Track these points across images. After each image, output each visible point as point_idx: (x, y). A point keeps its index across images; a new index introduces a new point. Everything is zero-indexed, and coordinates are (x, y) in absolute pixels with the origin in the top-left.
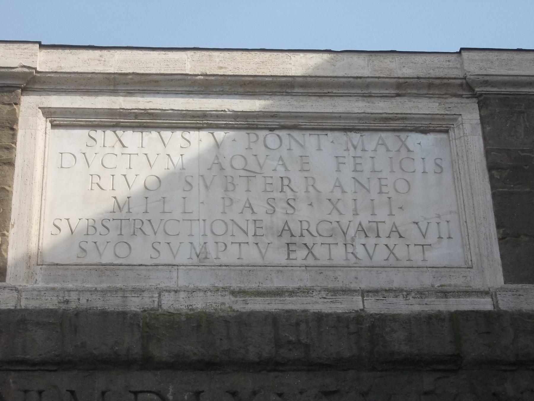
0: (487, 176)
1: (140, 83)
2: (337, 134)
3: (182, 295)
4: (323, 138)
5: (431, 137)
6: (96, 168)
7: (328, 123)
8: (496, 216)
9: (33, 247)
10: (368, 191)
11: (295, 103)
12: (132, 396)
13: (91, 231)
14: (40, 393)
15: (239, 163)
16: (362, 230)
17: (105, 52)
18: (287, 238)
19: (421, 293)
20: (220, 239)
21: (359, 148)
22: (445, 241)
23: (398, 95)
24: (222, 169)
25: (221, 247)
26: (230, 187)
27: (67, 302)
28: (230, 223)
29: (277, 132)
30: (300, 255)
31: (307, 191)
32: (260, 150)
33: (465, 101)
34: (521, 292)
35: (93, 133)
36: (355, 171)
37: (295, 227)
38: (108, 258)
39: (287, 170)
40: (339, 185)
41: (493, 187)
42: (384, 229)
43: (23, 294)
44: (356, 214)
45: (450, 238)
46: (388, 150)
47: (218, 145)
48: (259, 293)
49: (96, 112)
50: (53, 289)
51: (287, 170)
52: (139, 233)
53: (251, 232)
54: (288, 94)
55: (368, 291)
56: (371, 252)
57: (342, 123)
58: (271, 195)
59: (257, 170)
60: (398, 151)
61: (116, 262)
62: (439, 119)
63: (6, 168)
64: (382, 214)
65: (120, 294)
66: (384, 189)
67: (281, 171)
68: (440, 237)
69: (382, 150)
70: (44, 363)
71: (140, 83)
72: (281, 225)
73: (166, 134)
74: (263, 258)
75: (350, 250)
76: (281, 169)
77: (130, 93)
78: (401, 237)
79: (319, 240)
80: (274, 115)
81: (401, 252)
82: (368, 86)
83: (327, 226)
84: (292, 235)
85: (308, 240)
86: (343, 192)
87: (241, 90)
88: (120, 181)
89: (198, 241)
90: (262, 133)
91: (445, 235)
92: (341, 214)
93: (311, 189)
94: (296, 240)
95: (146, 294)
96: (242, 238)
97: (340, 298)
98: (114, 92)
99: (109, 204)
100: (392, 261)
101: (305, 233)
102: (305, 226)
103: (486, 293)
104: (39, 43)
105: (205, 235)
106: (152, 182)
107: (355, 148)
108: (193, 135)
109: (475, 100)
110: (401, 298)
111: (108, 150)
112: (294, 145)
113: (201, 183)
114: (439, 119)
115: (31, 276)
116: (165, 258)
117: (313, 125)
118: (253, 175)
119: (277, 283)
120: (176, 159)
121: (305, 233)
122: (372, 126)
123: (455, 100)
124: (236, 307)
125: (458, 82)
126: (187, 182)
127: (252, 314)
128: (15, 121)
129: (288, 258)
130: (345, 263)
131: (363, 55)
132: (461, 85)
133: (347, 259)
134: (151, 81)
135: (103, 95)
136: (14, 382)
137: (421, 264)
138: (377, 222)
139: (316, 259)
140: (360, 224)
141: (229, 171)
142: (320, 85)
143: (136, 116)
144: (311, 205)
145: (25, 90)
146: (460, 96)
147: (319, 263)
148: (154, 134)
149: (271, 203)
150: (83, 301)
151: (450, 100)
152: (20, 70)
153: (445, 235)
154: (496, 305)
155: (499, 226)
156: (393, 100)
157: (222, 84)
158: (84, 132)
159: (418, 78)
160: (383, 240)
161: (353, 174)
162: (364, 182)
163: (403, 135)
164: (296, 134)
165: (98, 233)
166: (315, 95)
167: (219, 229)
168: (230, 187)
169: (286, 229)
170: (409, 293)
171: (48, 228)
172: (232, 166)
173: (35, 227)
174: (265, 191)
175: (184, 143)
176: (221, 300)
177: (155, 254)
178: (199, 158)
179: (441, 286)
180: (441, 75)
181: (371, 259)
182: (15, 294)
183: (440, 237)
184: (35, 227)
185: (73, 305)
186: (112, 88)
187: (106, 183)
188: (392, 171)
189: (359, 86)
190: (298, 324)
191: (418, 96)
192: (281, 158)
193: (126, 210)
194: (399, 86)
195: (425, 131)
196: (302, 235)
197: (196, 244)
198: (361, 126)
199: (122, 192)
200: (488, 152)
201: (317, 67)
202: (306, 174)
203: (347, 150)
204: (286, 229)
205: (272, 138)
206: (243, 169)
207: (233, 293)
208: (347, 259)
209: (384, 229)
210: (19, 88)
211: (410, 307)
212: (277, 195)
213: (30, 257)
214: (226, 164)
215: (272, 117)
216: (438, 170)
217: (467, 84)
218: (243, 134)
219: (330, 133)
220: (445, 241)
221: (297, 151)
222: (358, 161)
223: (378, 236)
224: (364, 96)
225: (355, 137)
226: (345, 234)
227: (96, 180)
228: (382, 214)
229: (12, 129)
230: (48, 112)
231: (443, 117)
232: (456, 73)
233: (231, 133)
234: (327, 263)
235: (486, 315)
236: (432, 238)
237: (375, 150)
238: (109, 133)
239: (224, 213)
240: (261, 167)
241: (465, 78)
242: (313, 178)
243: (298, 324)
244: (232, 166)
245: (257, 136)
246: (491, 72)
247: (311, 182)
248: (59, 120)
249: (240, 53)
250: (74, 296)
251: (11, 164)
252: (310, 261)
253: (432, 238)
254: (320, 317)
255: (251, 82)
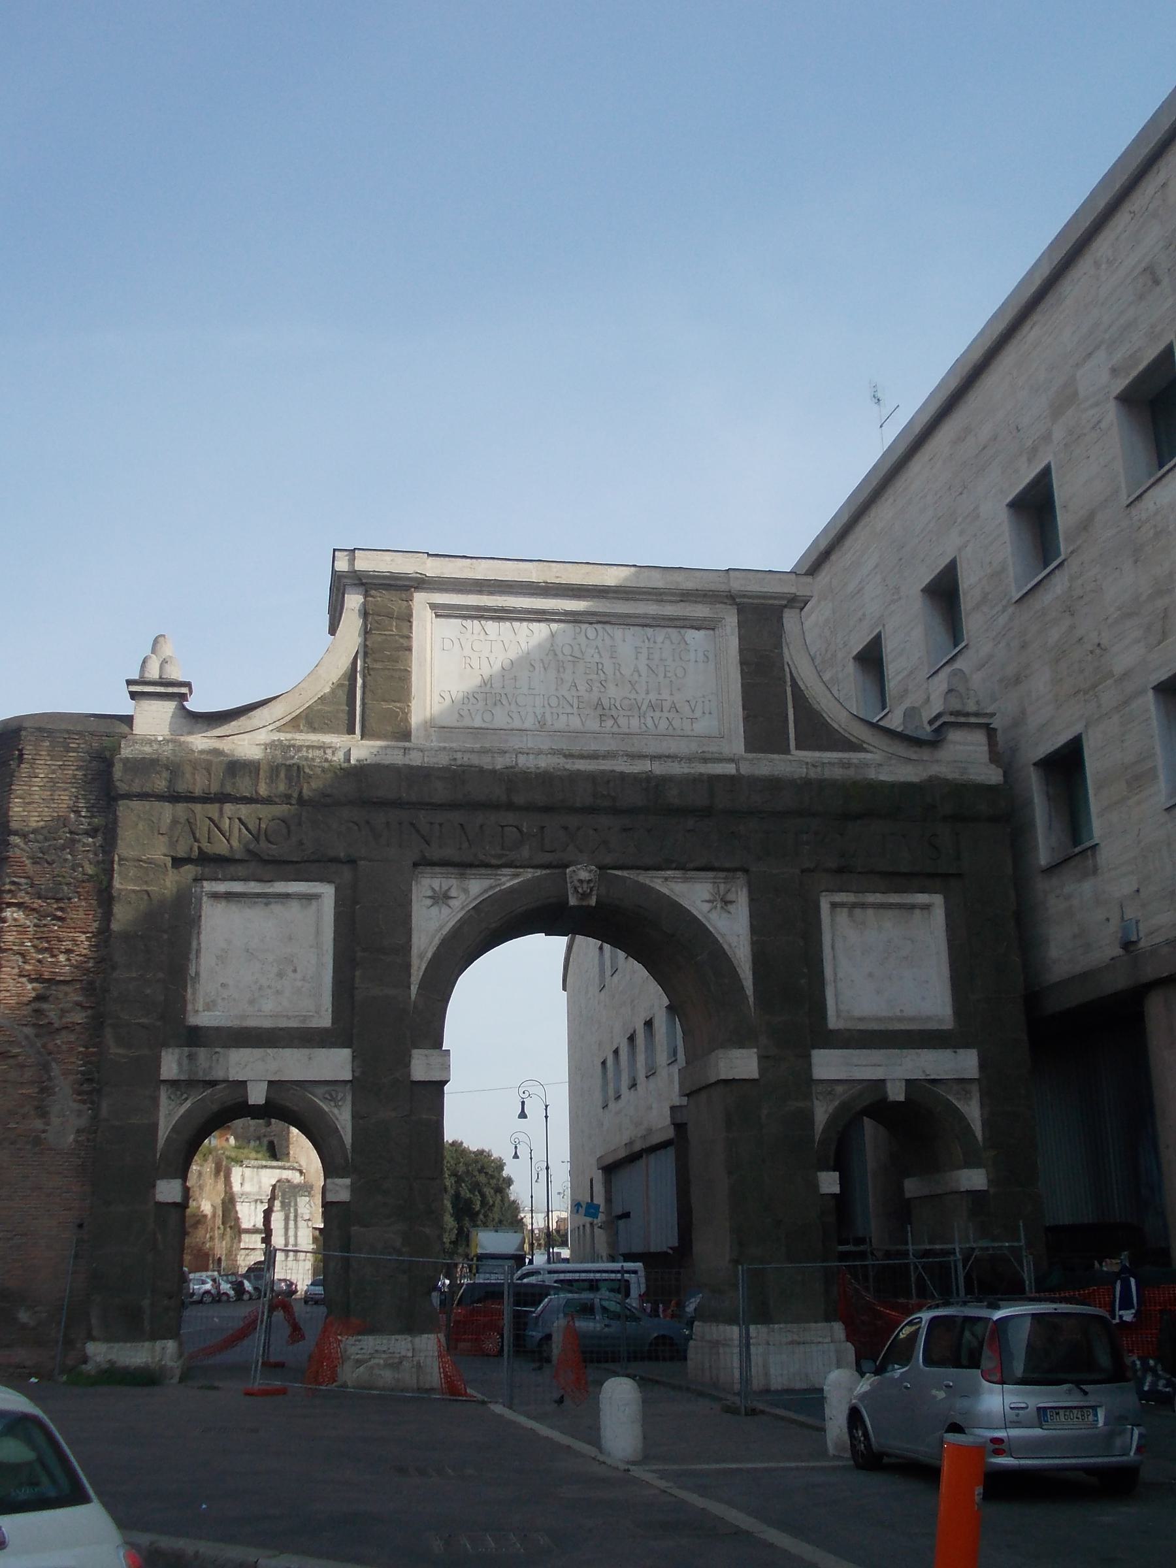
0: (739, 668)
1: (500, 586)
2: (637, 628)
3: (531, 757)
4: (627, 631)
5: (702, 632)
6: (467, 651)
7: (629, 621)
8: (743, 700)
9: (428, 715)
10: (657, 675)
11: (608, 605)
12: (500, 829)
13: (466, 701)
14: (441, 825)
15: (567, 650)
16: (651, 706)
17: (474, 560)
18: (600, 712)
19: (690, 759)
20: (554, 710)
21: (652, 640)
22: (707, 715)
23: (682, 601)
24: (556, 655)
25: (555, 717)
26: (561, 670)
27: (455, 759)
28: (561, 698)
29: (595, 626)
30: (609, 723)
31: (614, 674)
32: (582, 639)
33: (729, 607)
34: (755, 762)
35: (464, 622)
36: (648, 659)
37: (605, 702)
38: (478, 723)
39: (601, 657)
40: (637, 670)
41: (742, 678)
42: (666, 705)
43: (426, 753)
44: (647, 693)
45: (710, 713)
46: (672, 643)
47: (553, 635)
48: (582, 757)
49: (467, 607)
50: (445, 748)
51: (601, 657)
52: (498, 703)
53: (575, 706)
54: (604, 597)
55: (655, 757)
56: (657, 723)
57: (641, 621)
58: (590, 677)
59: (579, 655)
60: (679, 644)
61: (483, 726)
62: (709, 621)
63: (407, 652)
64: (665, 695)
65: (490, 755)
66: (669, 675)
67: (597, 658)
68: (704, 713)
69: (667, 642)
70: (440, 805)
71: (500, 586)
72: (596, 700)
73: (516, 624)
74: (583, 725)
75: (642, 721)
76: (597, 656)
77: (491, 593)
78: (677, 712)
79: (622, 713)
80: (593, 614)
81: (676, 723)
82: (661, 594)
83: (626, 702)
84: (604, 709)
85: (614, 712)
86: (640, 676)
87: (570, 593)
88: (485, 662)
89: (539, 711)
90: (584, 626)
91: (707, 711)
92: (637, 693)
93: (617, 672)
94: (607, 712)
95: (507, 755)
96: (569, 710)
97: (637, 762)
98: (480, 592)
99: (477, 681)
100: (671, 732)
101: (612, 706)
102: (613, 701)
103: (731, 760)
104: (427, 553)
105: (544, 707)
106: (507, 663)
107: (649, 640)
108: (535, 626)
109: (735, 607)
110: (676, 763)
111: (475, 637)
112: (606, 637)
113: (541, 665)
114: (709, 621)
115: (428, 737)
116: (517, 724)
117: (621, 621)
118: (576, 660)
119: (593, 746)
120: (524, 646)
121: (612, 706)
122: (662, 623)
123: (723, 606)
124: (568, 767)
125: (725, 594)
126: (531, 664)
127: (579, 773)
128: (411, 615)
129: (601, 726)
130: (638, 731)
131: (659, 570)
132: (727, 596)
133: (640, 728)
134: (507, 585)
135: (472, 594)
136: (424, 817)
137: (690, 733)
138: (662, 700)
139: (619, 727)
140: (650, 701)
141: (561, 657)
142: (626, 592)
143: (496, 611)
144: (617, 685)
145: (417, 588)
146: (725, 603)
147: (620, 731)
148: (508, 624)
149: (589, 682)
150: (465, 759)
151: (717, 606)
152: (415, 575)
153: (707, 711)
154: (738, 770)
155: (744, 709)
156: (678, 605)
157: (557, 589)
158: (459, 621)
159: (697, 590)
160: (666, 714)
161: (647, 662)
162: (654, 668)
163: (683, 631)
164: (608, 627)
165: (470, 704)
166: (622, 599)
167: (554, 702)
168: (561, 670)
169: (599, 704)
170: (682, 759)
171: (436, 698)
172: (562, 652)
173: (428, 698)
174: (585, 673)
175: (528, 632)
176: (558, 761)
177: (510, 720)
178: (540, 645)
179: (703, 752)
180: (713, 589)
181: (656, 727)
182: (421, 754)
183: (704, 713)
184: (428, 698)
185: (459, 762)
186: (479, 589)
187: (475, 664)
188: (674, 660)
189: (656, 594)
190: (608, 782)
191: (696, 602)
192: (597, 647)
193: (489, 686)
194: (683, 595)
195: (698, 629)
196: (610, 709)
197: (538, 713)
198: (654, 623)
199: (486, 672)
200: (741, 651)
201: (626, 579)
202: (614, 660)
203: (644, 642)
204: (599, 704)
205: (590, 630)
206: (571, 655)
207: (565, 756)
208: (640, 728)
209: (666, 705)
210: (412, 587)
211: (682, 770)
212: (594, 677)
213: (426, 723)
214: (559, 652)
215: (592, 614)
216: (706, 660)
217: (731, 596)
218: (571, 625)
219: (631, 628)
220: (707, 715)
221: (608, 642)
222: (651, 651)
223: (662, 711)
224: (657, 601)
225: (649, 631)
226: (639, 709)
227: (468, 660)
228: (665, 695)
229: (410, 622)
230: (433, 606)
231: (712, 620)
232: (723, 587)
233: (562, 625)
234: (627, 731)
235: (732, 778)
236: (698, 714)
237: (663, 643)
238: (476, 622)
239: (557, 689)
240: (583, 655)
241: (730, 592)
242: (619, 665)
243: (608, 782)
244: (562, 652)
245: (580, 628)
246: (749, 588)
247: (617, 666)
248: (440, 612)
249: (571, 564)
250: (459, 756)
251: (409, 649)
252: (615, 729)
253: (698, 714)
254: (623, 776)
255: (578, 589)
